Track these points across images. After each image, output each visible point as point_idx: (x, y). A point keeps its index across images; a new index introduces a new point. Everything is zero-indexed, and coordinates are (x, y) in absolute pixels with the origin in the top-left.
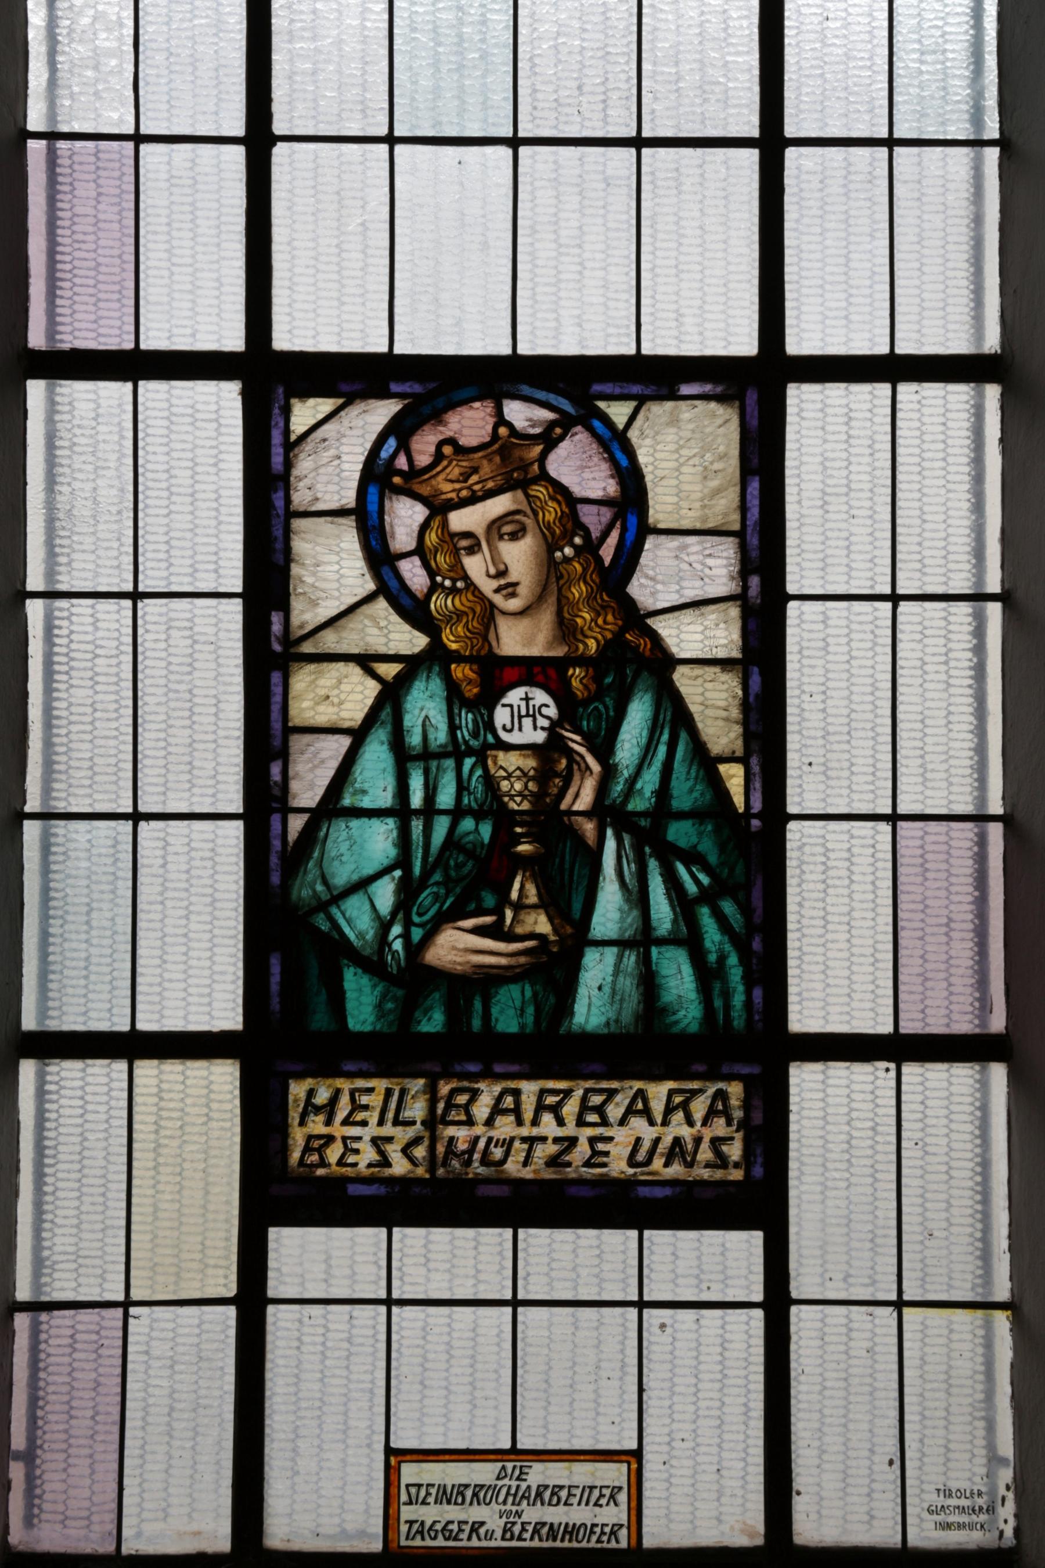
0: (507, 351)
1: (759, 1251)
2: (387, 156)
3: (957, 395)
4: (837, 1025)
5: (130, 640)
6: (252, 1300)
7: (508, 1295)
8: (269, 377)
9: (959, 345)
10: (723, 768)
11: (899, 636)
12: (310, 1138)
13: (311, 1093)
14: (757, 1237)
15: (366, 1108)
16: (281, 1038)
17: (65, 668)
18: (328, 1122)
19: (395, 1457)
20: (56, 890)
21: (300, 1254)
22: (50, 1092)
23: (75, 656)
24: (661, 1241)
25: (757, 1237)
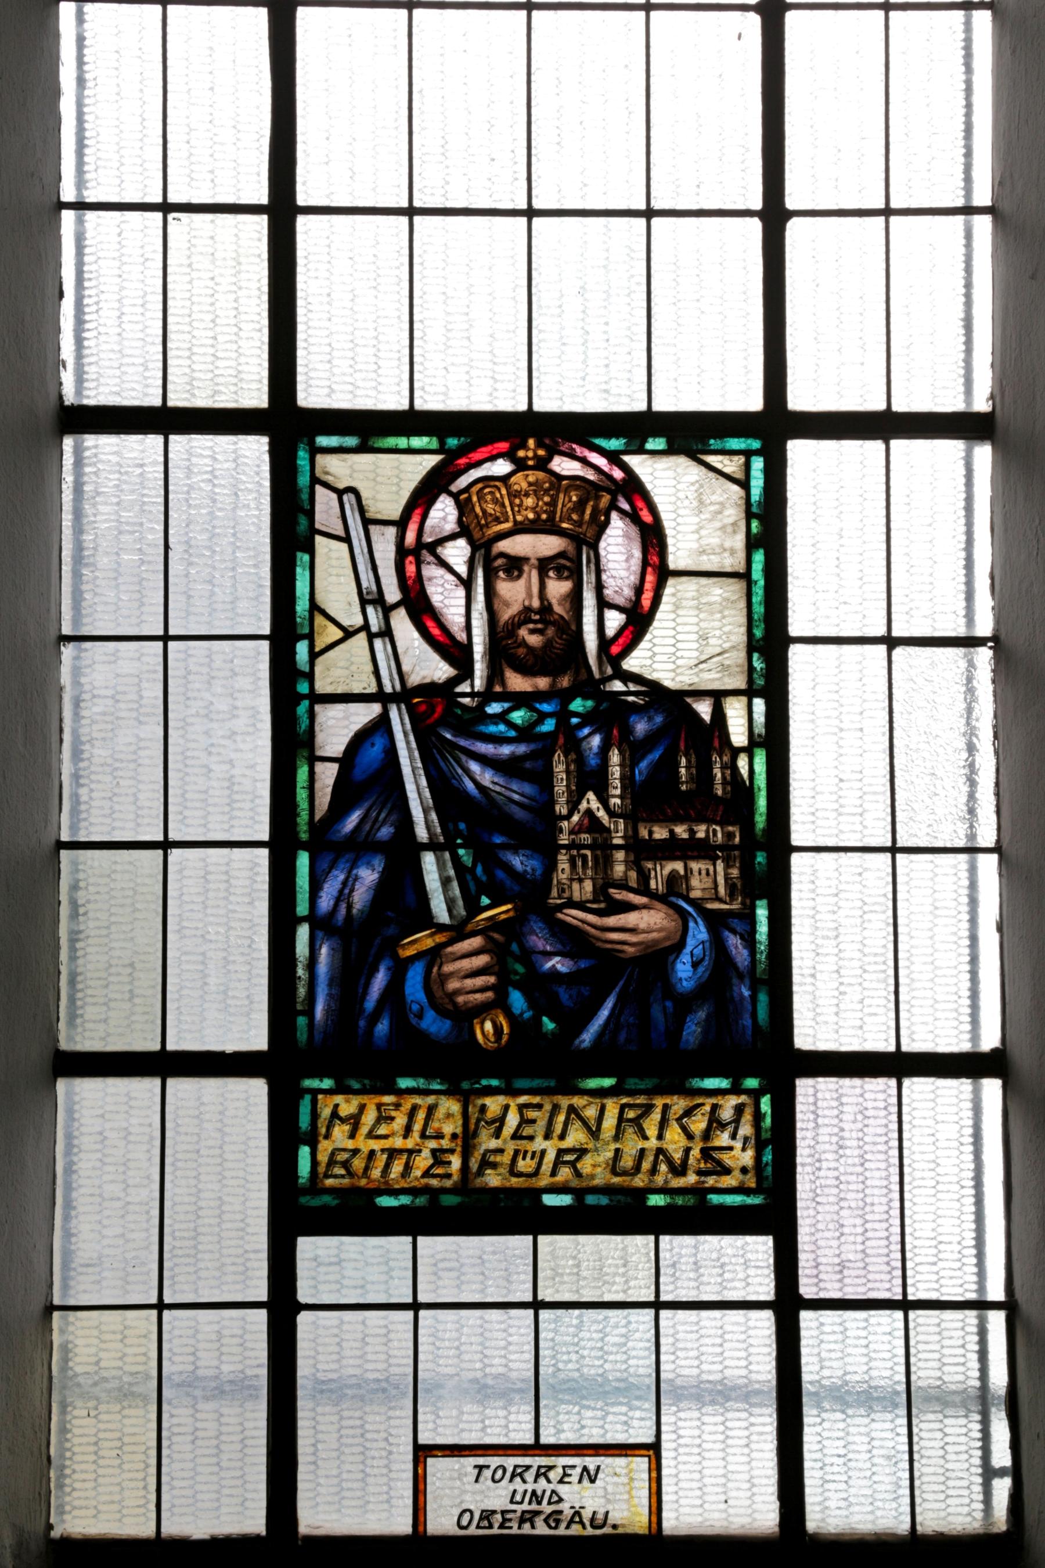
0: (523, 407)
2: (161, 224)
3: (949, 451)
6: (283, 1306)
7: (154, 1300)
8: (288, 426)
9: (951, 402)
12: (561, 1152)
15: (533, 1121)
16: (300, 1059)
18: (352, 1136)
19: (422, 1453)
23: (102, 693)
24: (677, 1247)
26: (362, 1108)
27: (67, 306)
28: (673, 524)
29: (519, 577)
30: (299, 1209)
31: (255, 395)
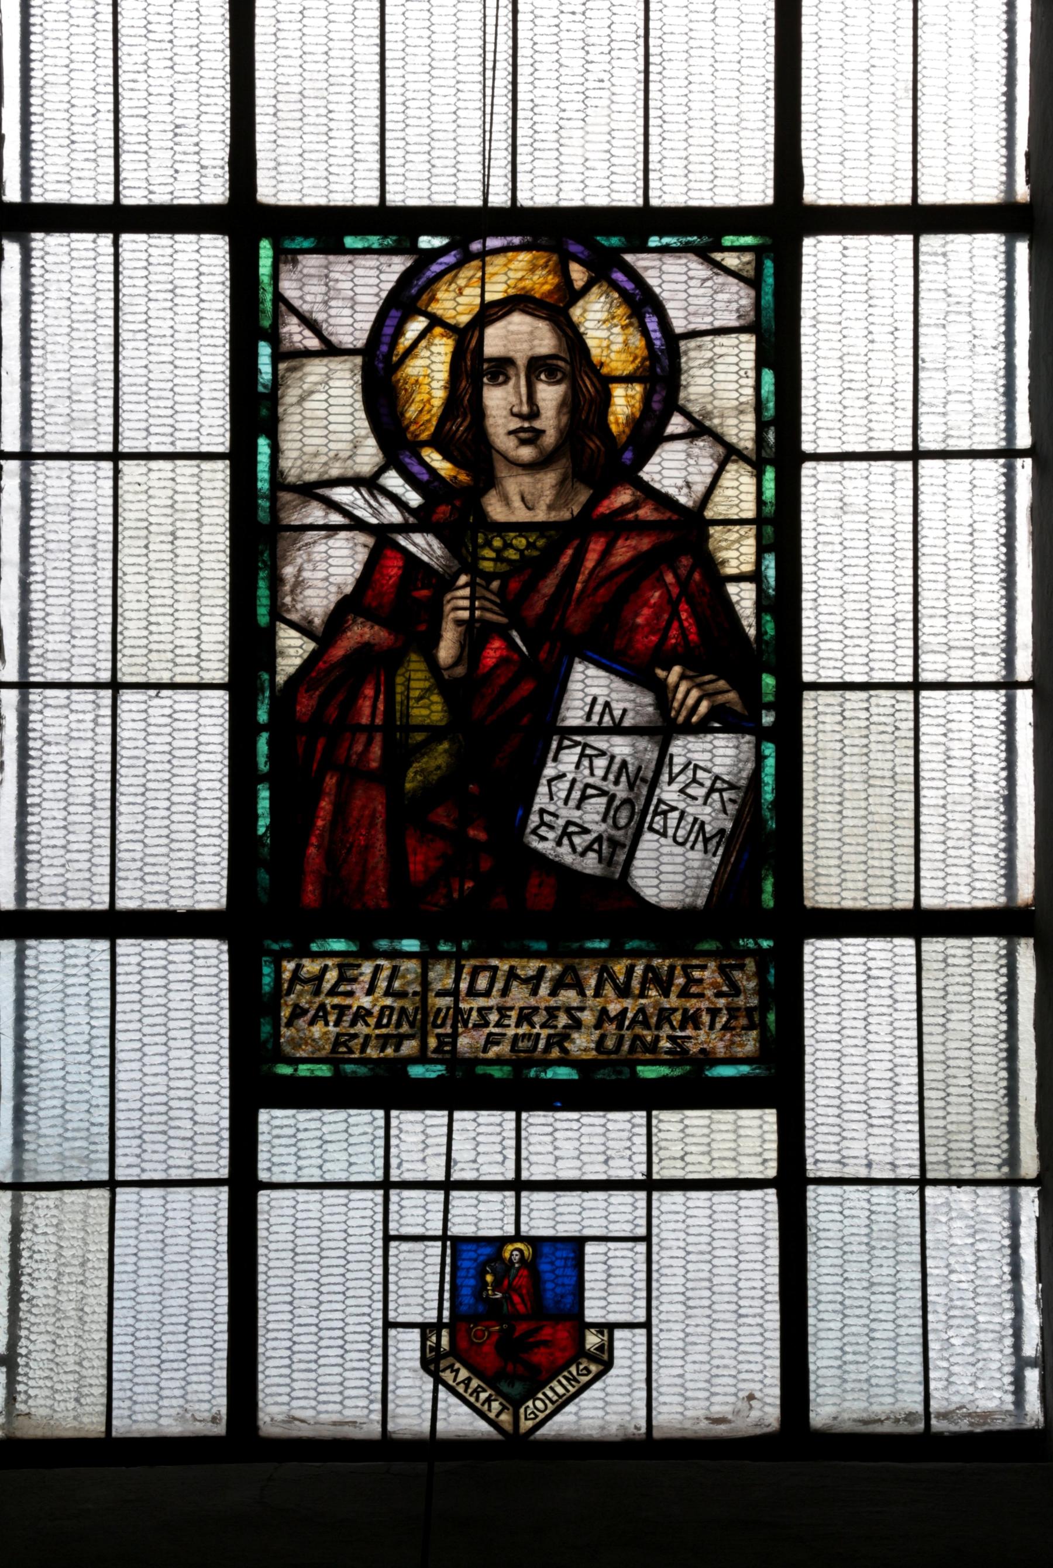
1: (774, 1207)
4: (856, 197)
5: (109, 601)
6: (244, 1184)
8: (248, 223)
10: (732, 589)
11: (921, 277)
13: (299, 967)
14: (770, 1116)
17: (41, 633)
20: (33, 852)
21: (291, 1138)
22: (29, 1067)
24: (669, 1122)
25: (770, 1116)
26: (325, 969)
27: (1022, 146)
28: (357, 424)
29: (506, 382)
30: (258, 1080)
31: (216, 191)
